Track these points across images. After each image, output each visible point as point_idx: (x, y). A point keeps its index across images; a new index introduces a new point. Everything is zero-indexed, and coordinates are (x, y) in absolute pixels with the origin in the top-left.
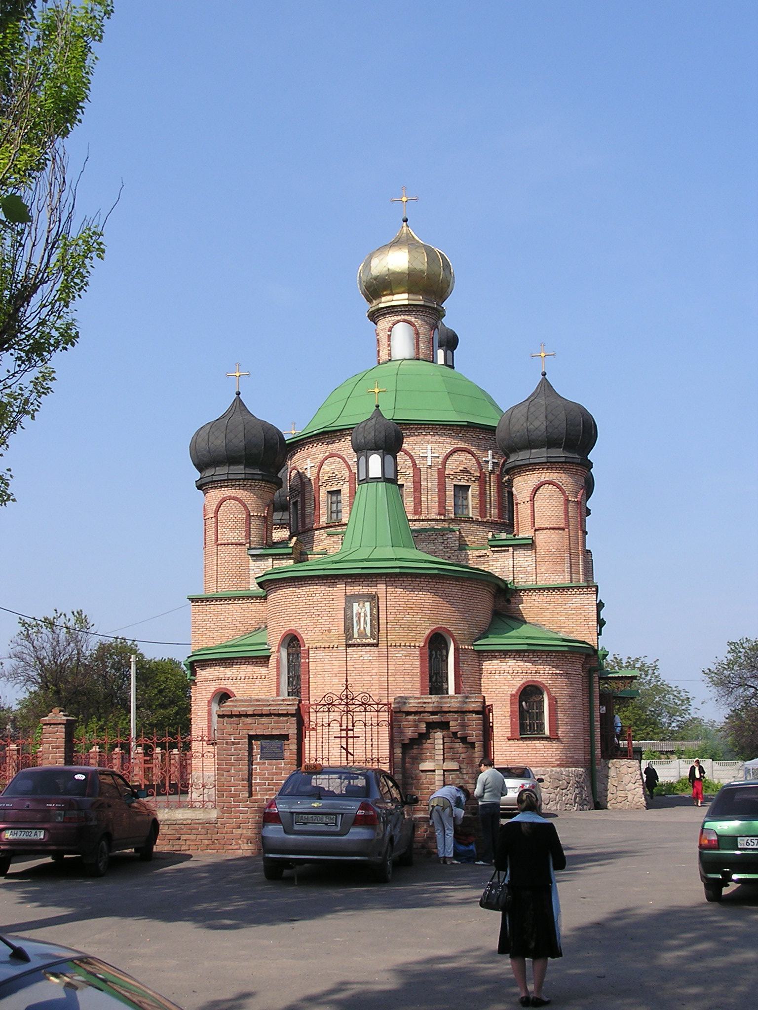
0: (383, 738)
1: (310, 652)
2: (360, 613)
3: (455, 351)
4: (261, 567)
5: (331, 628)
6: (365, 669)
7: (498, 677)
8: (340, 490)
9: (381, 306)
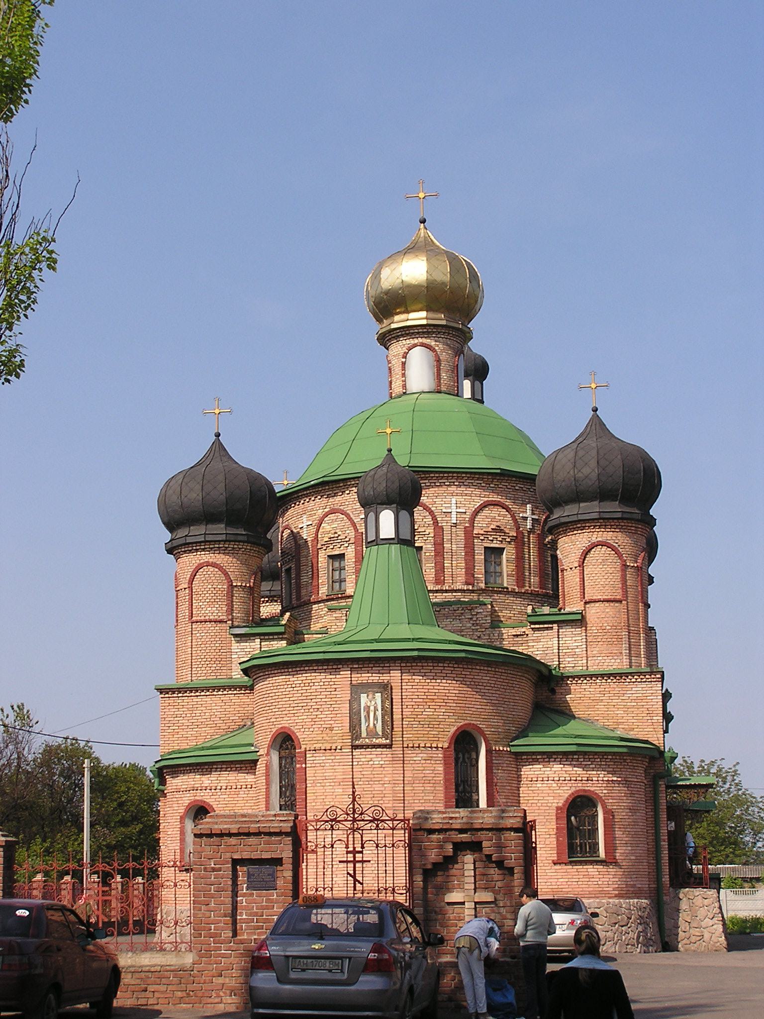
2: (369, 707)
3: (484, 382)
4: (246, 650)
5: (333, 726)
7: (541, 785)
9: (394, 326)
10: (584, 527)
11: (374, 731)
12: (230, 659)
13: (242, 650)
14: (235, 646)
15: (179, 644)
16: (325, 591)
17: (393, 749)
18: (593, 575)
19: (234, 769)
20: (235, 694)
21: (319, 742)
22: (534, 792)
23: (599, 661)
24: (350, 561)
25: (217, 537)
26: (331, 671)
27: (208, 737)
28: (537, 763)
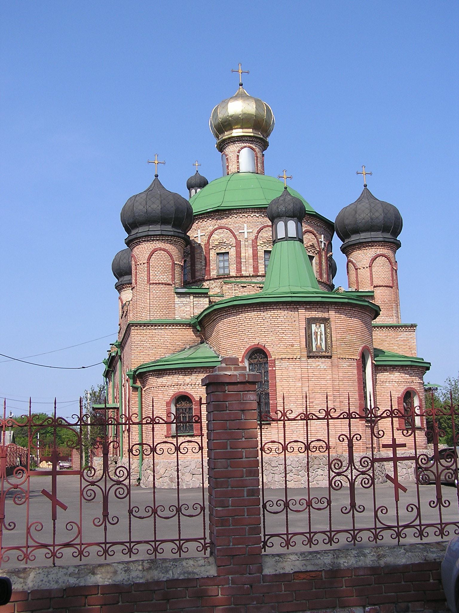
0: (337, 429)
1: (276, 362)
2: (317, 332)
4: (184, 303)
5: (294, 343)
6: (322, 375)
8: (228, 252)
10: (373, 245)
11: (321, 348)
12: (174, 308)
13: (182, 303)
14: (177, 300)
15: (138, 297)
16: (215, 273)
17: (332, 359)
18: (378, 272)
19: (209, 372)
20: (179, 329)
21: (285, 353)
22: (385, 388)
23: (382, 319)
24: (232, 256)
25: (168, 233)
26: (291, 309)
27: (162, 355)
28: (386, 371)
